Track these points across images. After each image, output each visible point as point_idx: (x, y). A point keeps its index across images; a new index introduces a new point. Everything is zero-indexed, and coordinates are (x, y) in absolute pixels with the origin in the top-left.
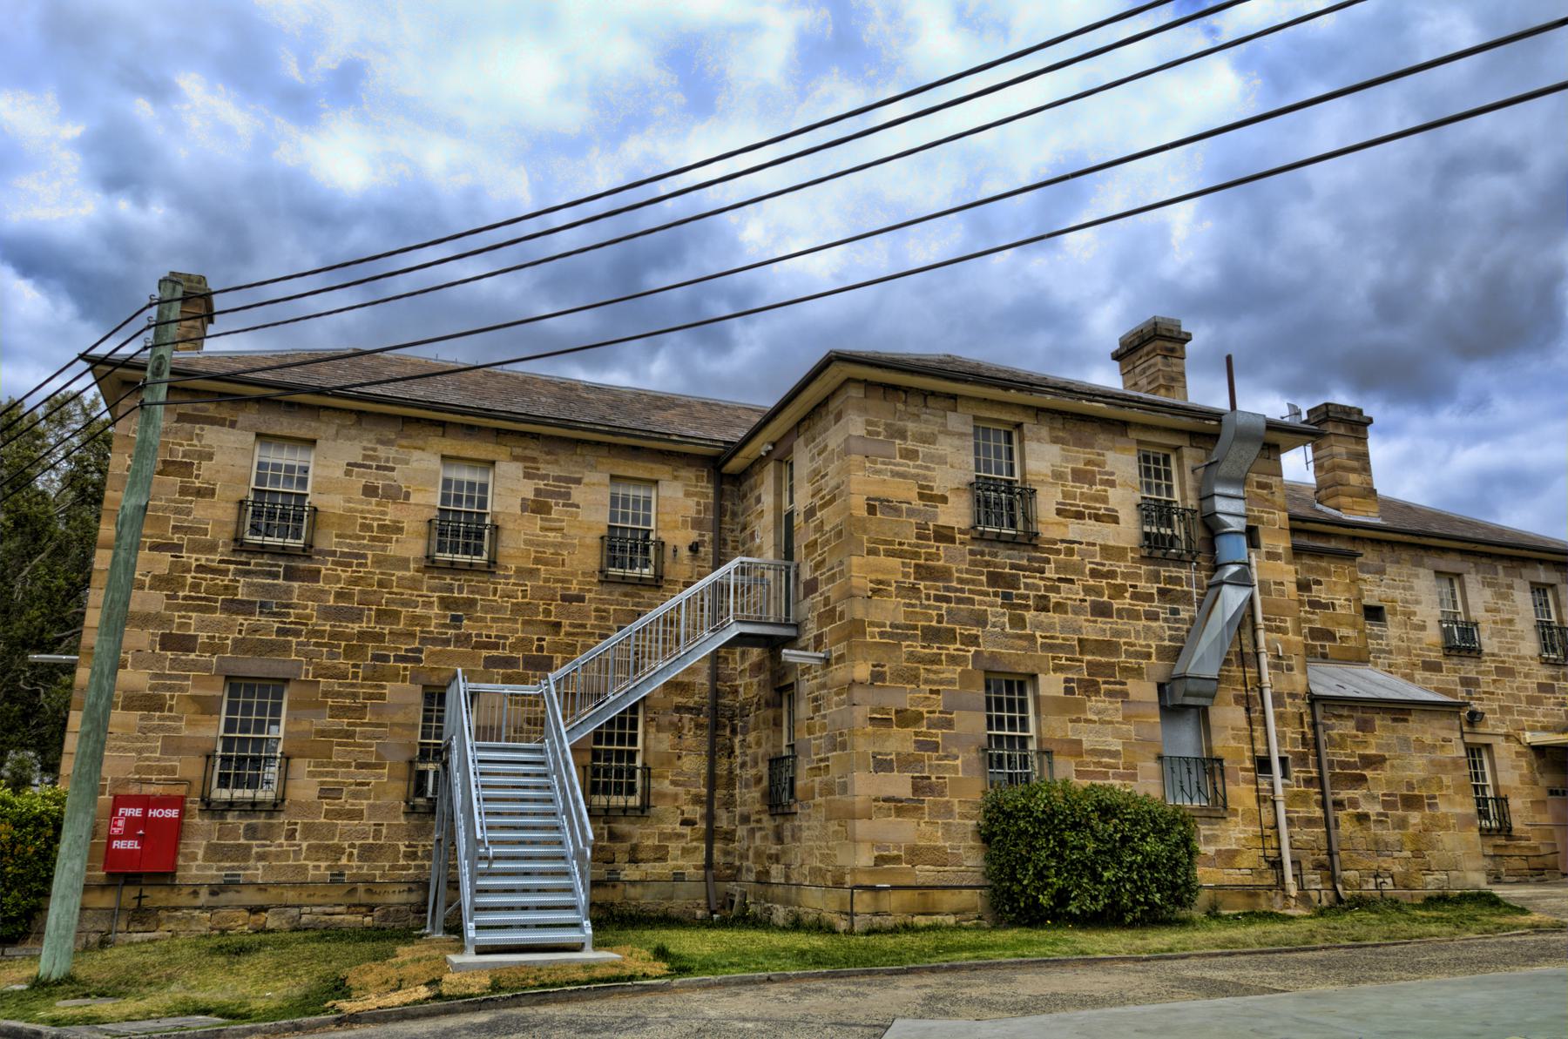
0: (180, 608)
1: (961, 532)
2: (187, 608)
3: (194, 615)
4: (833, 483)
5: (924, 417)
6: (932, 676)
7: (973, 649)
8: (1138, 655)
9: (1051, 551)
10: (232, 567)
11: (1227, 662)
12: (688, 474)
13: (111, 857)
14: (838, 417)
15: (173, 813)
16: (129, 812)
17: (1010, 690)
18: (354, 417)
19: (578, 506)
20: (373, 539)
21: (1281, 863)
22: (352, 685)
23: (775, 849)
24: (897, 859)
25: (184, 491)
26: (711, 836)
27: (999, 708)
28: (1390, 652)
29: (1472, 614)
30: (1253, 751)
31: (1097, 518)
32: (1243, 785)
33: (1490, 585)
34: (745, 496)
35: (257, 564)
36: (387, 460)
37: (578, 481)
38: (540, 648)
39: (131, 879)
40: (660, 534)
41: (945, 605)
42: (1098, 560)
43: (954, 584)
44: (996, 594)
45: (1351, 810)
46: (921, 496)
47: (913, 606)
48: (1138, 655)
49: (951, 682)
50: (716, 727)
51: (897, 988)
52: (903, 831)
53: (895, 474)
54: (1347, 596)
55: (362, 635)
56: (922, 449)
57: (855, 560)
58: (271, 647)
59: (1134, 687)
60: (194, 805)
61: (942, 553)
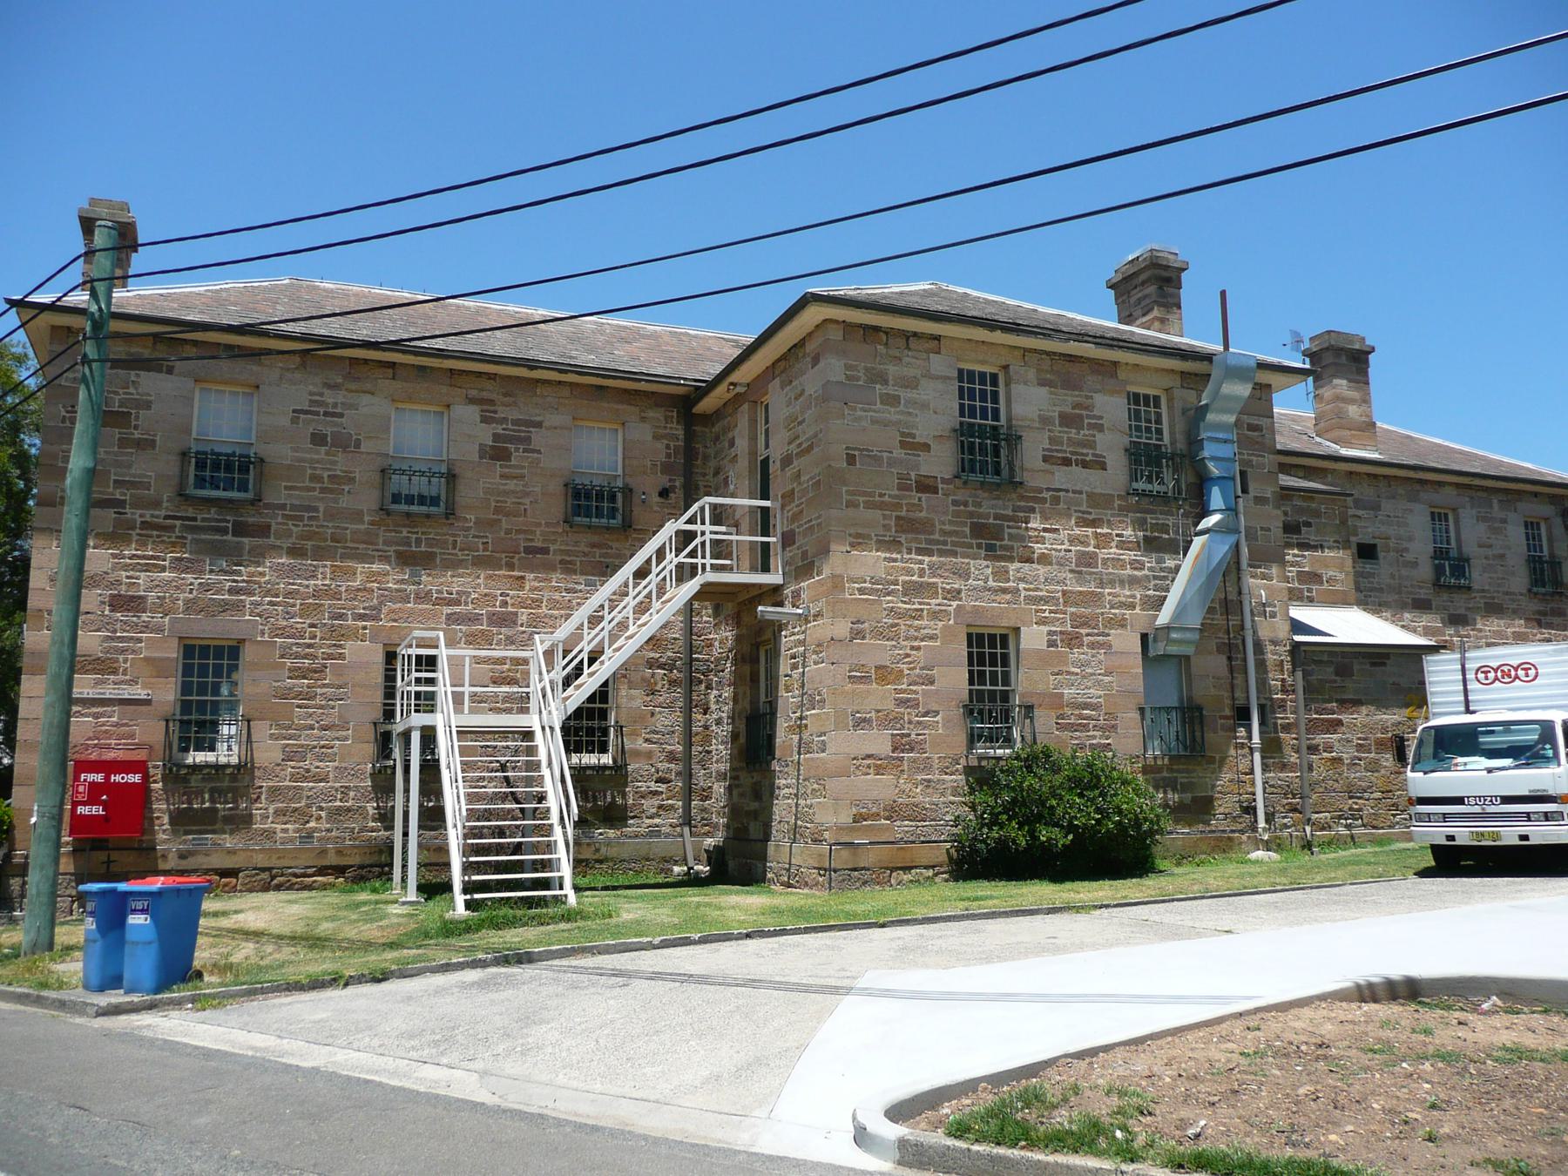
0: (126, 567)
1: (944, 481)
2: (134, 568)
3: (142, 574)
4: (811, 433)
5: (906, 359)
6: (912, 632)
7: (954, 604)
8: (1122, 605)
9: (1035, 499)
10: (178, 523)
11: (1211, 610)
12: (656, 414)
13: (79, 823)
14: (816, 360)
15: (135, 778)
16: (92, 777)
17: (993, 645)
18: (297, 359)
19: (539, 452)
20: (323, 490)
21: (1255, 809)
22: (309, 646)
23: (754, 805)
24: (877, 816)
25: (123, 443)
26: (688, 793)
27: (981, 663)
28: (1381, 590)
29: (1465, 550)
30: (1233, 698)
31: (1085, 465)
32: (1221, 733)
33: (1484, 519)
34: (717, 438)
35: (204, 520)
36: (335, 405)
37: (539, 425)
38: (505, 604)
39: (99, 845)
40: (628, 480)
41: (927, 559)
42: (1084, 508)
43: (937, 536)
44: (979, 546)
45: (1325, 755)
46: (903, 445)
47: (895, 560)
48: (1122, 605)
49: (932, 638)
50: (691, 682)
51: (871, 941)
52: (881, 788)
53: (874, 421)
54: (1337, 537)
55: (317, 594)
56: (904, 394)
57: (834, 512)
58: (225, 607)
59: (1117, 638)
60: (156, 772)
61: (924, 504)
